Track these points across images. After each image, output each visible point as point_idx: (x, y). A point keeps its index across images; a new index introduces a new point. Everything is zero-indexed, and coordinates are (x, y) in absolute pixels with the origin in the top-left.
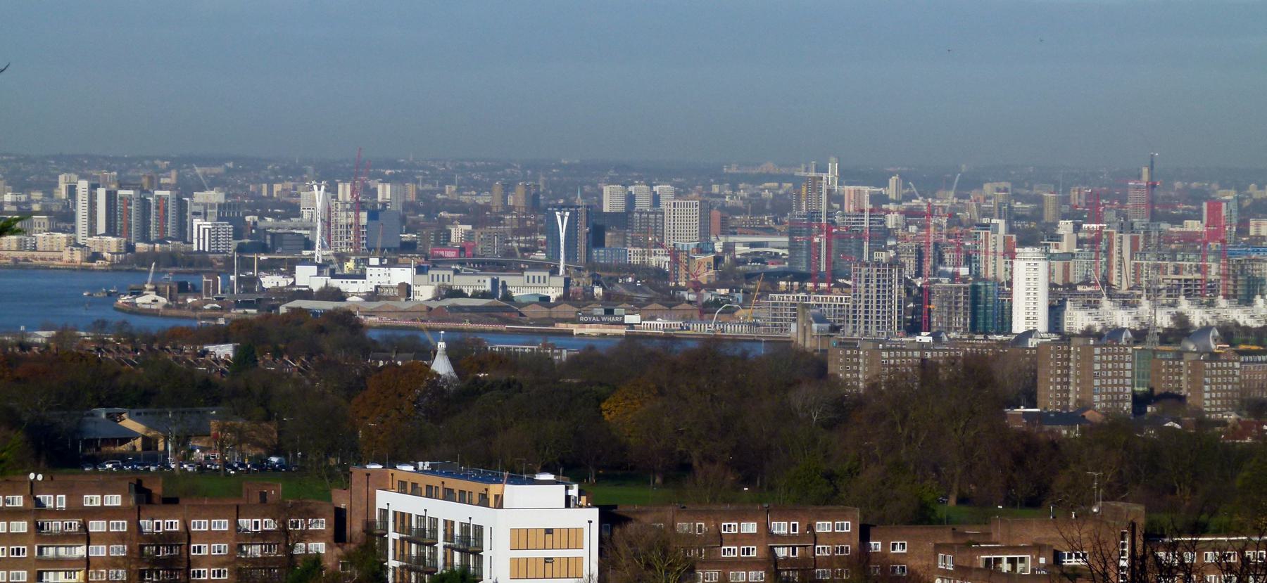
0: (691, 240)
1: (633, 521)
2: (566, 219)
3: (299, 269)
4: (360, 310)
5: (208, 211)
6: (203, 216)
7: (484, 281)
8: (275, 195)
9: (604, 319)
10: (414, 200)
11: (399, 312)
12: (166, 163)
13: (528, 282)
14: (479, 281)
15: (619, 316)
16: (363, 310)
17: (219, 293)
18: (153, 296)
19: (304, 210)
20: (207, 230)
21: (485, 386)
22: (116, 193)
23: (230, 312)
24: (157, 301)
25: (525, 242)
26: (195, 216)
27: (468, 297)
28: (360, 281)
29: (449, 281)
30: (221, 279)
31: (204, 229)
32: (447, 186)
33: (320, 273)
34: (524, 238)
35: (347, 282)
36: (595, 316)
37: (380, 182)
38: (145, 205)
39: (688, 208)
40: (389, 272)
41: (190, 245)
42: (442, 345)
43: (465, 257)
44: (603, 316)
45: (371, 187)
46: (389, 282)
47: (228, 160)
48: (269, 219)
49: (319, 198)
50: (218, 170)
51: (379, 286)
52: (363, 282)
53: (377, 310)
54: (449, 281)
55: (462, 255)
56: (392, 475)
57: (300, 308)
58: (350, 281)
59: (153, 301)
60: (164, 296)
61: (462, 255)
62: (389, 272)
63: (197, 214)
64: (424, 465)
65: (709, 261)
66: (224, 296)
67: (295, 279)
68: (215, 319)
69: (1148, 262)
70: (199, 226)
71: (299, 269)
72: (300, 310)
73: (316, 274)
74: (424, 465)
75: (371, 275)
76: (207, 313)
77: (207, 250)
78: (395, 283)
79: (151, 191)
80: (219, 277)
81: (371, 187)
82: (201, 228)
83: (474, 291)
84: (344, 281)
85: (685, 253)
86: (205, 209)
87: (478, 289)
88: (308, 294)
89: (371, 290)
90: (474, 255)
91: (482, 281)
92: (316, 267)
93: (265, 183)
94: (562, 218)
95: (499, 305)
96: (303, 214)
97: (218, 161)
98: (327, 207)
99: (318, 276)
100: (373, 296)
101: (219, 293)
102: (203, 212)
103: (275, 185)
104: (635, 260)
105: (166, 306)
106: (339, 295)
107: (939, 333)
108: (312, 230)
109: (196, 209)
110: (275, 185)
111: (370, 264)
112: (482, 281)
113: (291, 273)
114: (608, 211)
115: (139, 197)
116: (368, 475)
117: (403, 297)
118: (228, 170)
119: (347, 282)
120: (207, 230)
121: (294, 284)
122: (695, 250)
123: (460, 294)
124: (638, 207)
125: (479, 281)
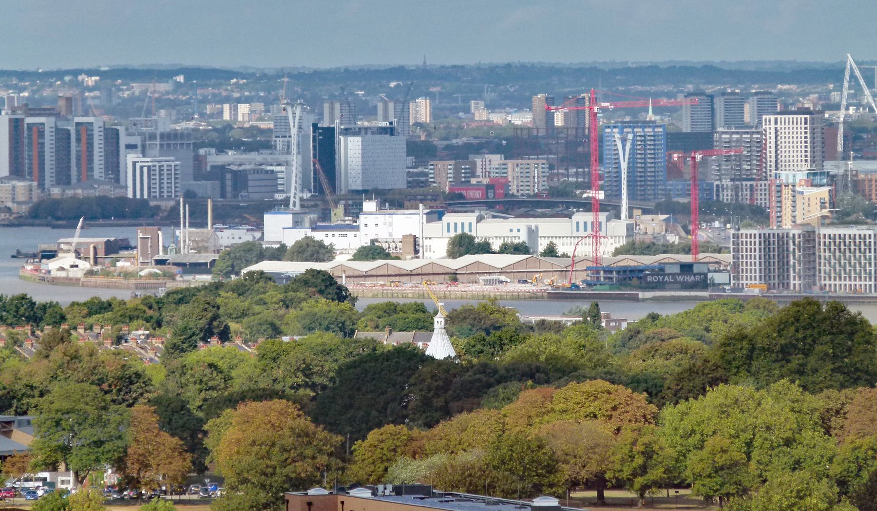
0: (799, 168)
2: (628, 146)
3: (269, 219)
4: (348, 273)
5: (148, 143)
6: (140, 149)
7: (518, 230)
8: (240, 119)
9: (680, 278)
10: (428, 122)
12: (93, 78)
13: (578, 230)
14: (511, 230)
15: (700, 274)
16: (351, 274)
18: (71, 259)
19: (278, 139)
20: (145, 170)
21: (497, 376)
22: (22, 120)
24: (77, 266)
25: (577, 175)
26: (129, 150)
27: (494, 253)
28: (351, 234)
30: (163, 235)
31: (142, 168)
32: (473, 102)
33: (297, 224)
34: (574, 170)
35: (333, 235)
36: (668, 275)
38: (63, 137)
39: (787, 126)
40: (390, 220)
41: (123, 190)
43: (494, 197)
44: (678, 274)
45: (370, 105)
46: (390, 234)
47: (177, 73)
49: (294, 123)
50: (163, 87)
51: (377, 240)
53: (373, 273)
56: (343, 503)
58: (337, 233)
59: (72, 266)
60: (86, 259)
61: (491, 195)
62: (390, 220)
63: (131, 147)
64: (385, 489)
65: (823, 197)
67: (263, 233)
68: (156, 287)
69: (819, 130)
70: (134, 163)
71: (269, 219)
73: (291, 226)
74: (385, 489)
76: (143, 281)
77: (146, 196)
78: (398, 236)
79: (70, 117)
80: (160, 233)
81: (370, 105)
82: (138, 166)
84: (330, 233)
85: (790, 187)
86: (144, 141)
87: (509, 241)
88: (279, 253)
89: (366, 245)
90: (506, 195)
91: (515, 230)
92: (291, 216)
93: (558, 128)
94: (624, 141)
97: (165, 74)
99: (294, 227)
100: (372, 252)
102: (139, 145)
104: (763, 202)
105: (90, 273)
106: (322, 252)
107: (74, 401)
108: (287, 165)
109: (132, 140)
112: (515, 230)
113: (259, 225)
114: (689, 131)
115: (53, 125)
116: (310, 504)
117: (409, 253)
118: (178, 85)
119: (333, 235)
120: (145, 170)
122: (803, 183)
123: (485, 248)
125: (511, 230)
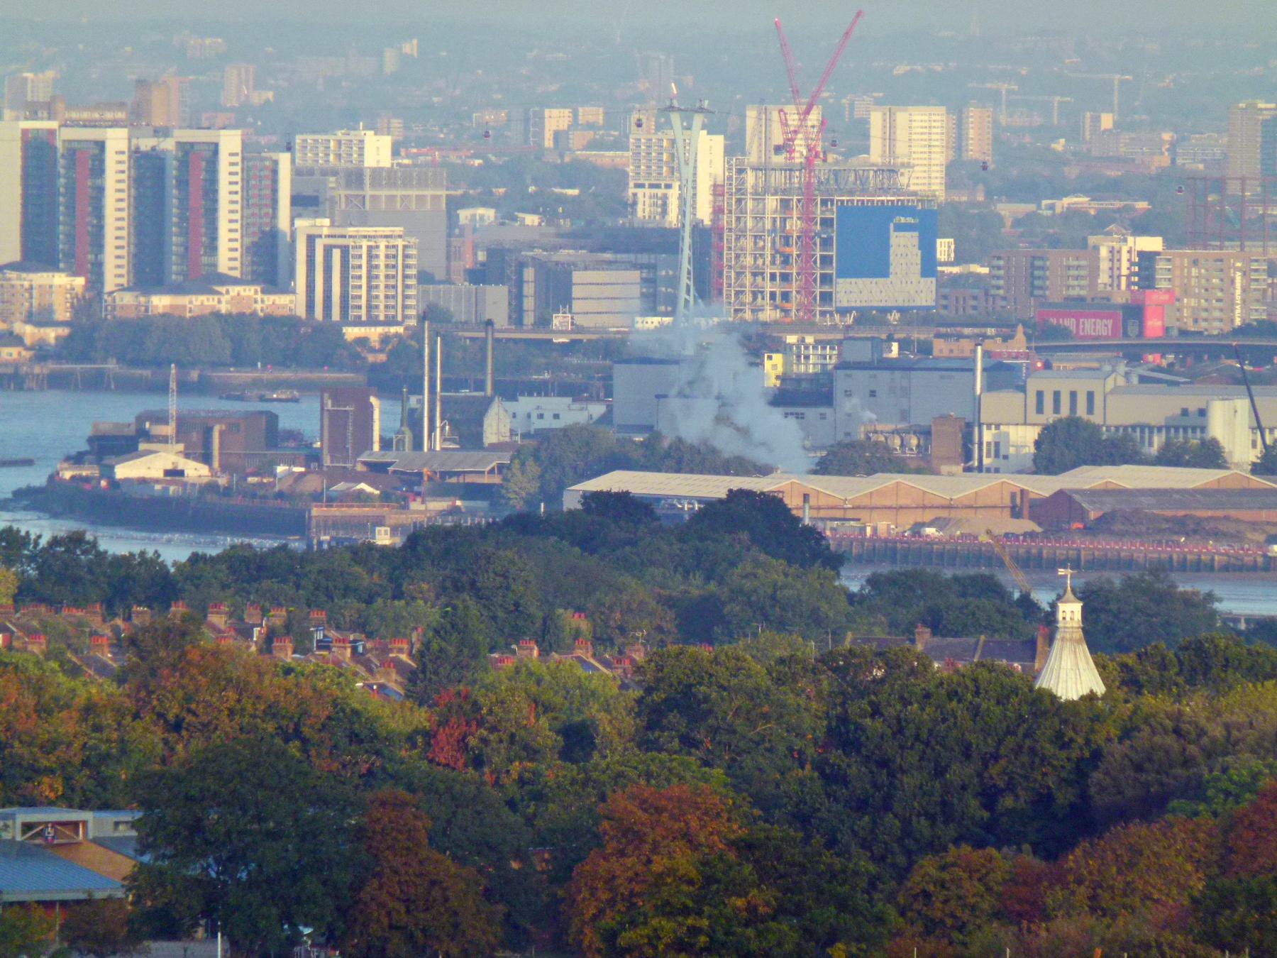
1: (1094, 746)
11: (932, 507)
17: (376, 447)
19: (640, 191)
23: (406, 507)
29: (1090, 410)
31: (328, 250)
37: (878, 103)
42: (1071, 612)
48: (531, 220)
52: (823, 416)
54: (1090, 410)
55: (1133, 330)
57: (627, 493)
66: (388, 457)
72: (623, 503)
75: (556, 416)
83: (1167, 445)
95: (1253, 485)
96: (635, 203)
98: (650, 355)
101: (376, 447)
103: (547, 112)
110: (547, 112)
111: (869, 343)
121: (606, 419)
124: (507, 439)
